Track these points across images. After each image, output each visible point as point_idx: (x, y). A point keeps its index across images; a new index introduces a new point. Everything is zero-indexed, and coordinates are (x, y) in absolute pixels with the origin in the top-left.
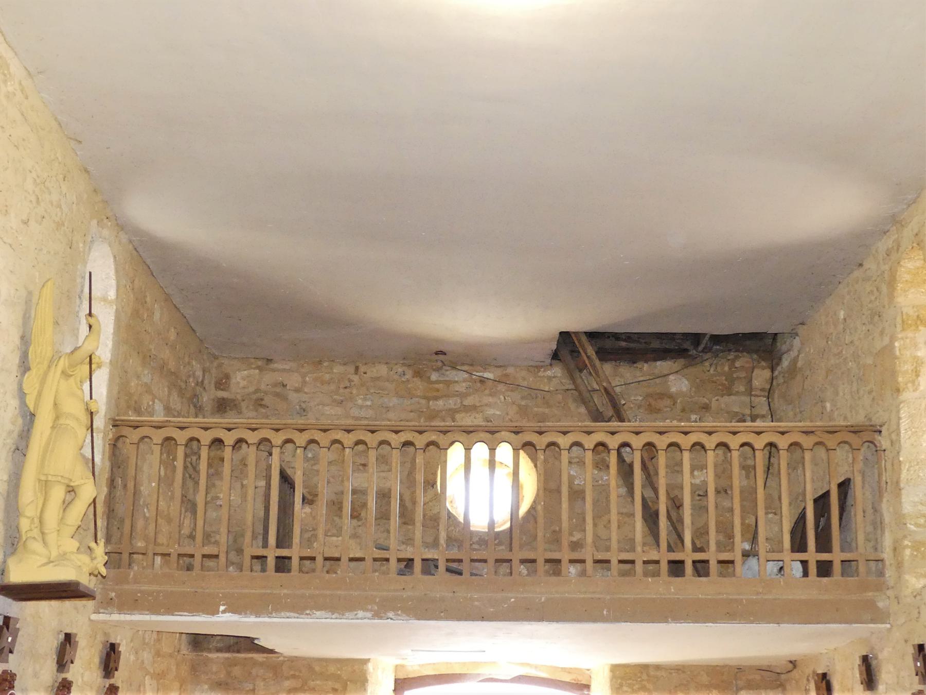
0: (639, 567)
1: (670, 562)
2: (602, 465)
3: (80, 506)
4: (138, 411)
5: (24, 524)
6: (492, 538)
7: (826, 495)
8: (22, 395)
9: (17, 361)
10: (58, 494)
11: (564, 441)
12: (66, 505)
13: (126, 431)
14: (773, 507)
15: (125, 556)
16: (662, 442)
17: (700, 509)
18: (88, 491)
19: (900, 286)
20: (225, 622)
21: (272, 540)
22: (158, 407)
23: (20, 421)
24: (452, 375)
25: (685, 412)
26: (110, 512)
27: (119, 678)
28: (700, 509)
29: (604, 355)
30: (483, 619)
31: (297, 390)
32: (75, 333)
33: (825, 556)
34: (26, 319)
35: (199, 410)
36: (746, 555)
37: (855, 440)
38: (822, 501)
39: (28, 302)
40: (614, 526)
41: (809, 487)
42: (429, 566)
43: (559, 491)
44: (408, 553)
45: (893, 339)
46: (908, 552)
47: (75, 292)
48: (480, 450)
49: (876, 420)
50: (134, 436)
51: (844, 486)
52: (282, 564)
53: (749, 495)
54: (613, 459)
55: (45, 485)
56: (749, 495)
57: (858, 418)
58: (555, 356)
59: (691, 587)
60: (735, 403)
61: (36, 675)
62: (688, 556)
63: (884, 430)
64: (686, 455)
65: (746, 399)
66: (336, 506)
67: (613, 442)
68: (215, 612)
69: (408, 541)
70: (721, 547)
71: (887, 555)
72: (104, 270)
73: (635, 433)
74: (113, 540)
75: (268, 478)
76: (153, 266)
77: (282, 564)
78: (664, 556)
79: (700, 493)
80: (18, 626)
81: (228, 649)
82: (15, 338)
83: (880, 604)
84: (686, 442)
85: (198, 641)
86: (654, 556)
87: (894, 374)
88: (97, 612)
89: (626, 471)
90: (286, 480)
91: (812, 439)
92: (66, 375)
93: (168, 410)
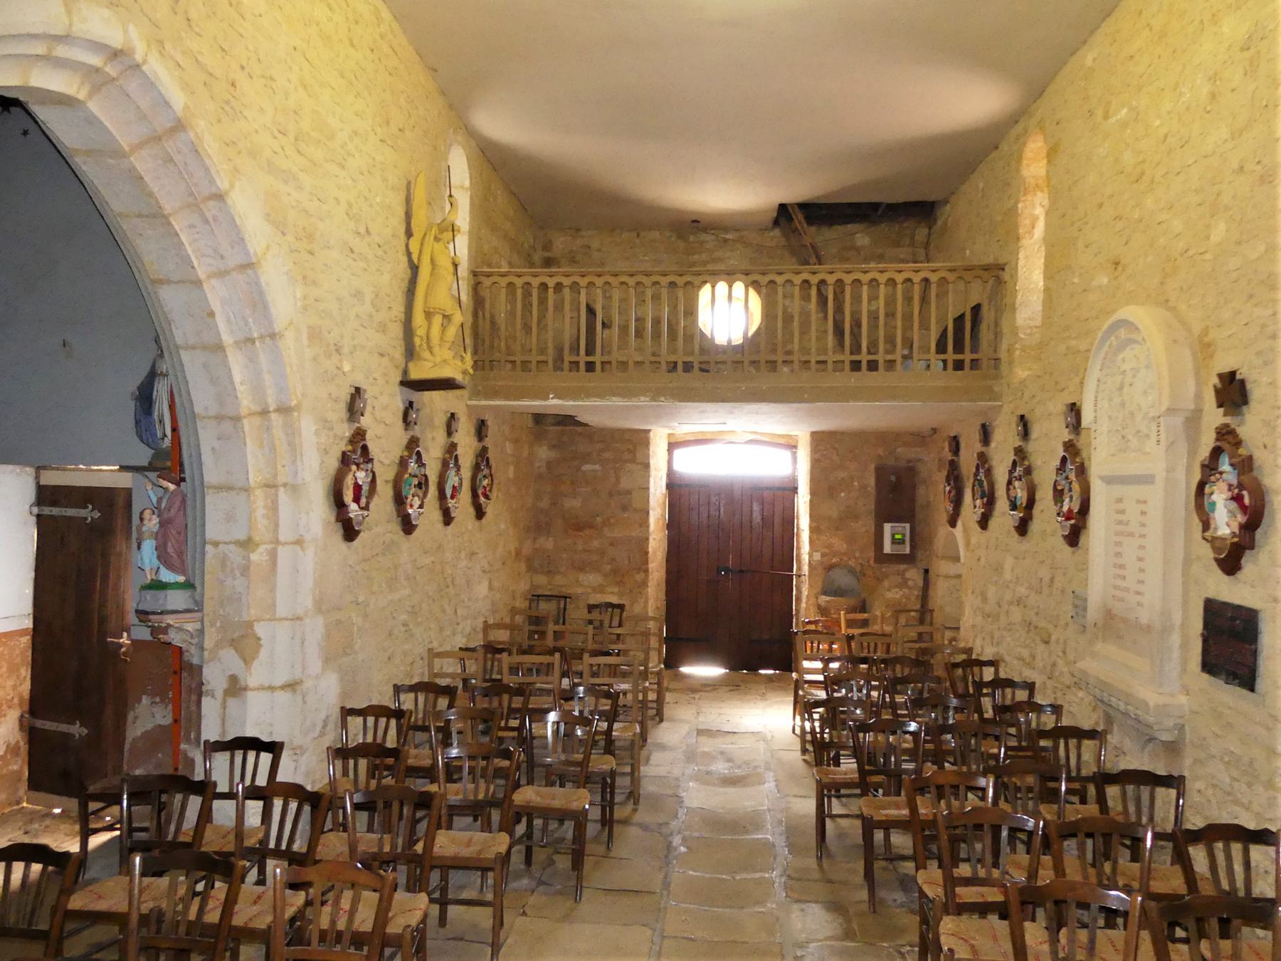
0: (830, 366)
1: (852, 362)
2: (806, 298)
3: (452, 331)
4: (489, 266)
5: (417, 341)
6: (731, 349)
7: (962, 317)
8: (409, 254)
9: (403, 230)
10: (437, 320)
11: (780, 280)
12: (444, 328)
13: (482, 279)
14: (925, 326)
15: (487, 363)
16: (848, 279)
17: (874, 326)
18: (458, 318)
19: (1025, 162)
20: (553, 404)
21: (582, 351)
22: (504, 263)
23: (409, 271)
24: (704, 237)
25: (866, 260)
26: (476, 335)
27: (488, 442)
28: (874, 326)
29: (810, 220)
30: (723, 401)
31: (599, 250)
32: (443, 208)
33: (959, 357)
34: (408, 201)
35: (532, 265)
36: (905, 357)
37: (985, 274)
38: (959, 320)
39: (408, 189)
40: (814, 339)
41: (950, 309)
42: (688, 367)
43: (776, 317)
44: (672, 358)
45: (1017, 202)
46: (1017, 352)
47: (441, 180)
48: (722, 287)
49: (1001, 261)
50: (487, 282)
51: (976, 309)
52: (590, 367)
53: (908, 317)
54: (814, 292)
55: (428, 315)
56: (908, 317)
57: (990, 260)
58: (776, 222)
59: (866, 378)
60: (903, 252)
61: (433, 439)
62: (864, 357)
63: (1007, 268)
64: (865, 288)
65: (910, 250)
66: (624, 329)
67: (814, 280)
68: (547, 398)
69: (673, 350)
70: (887, 352)
71: (1003, 355)
72: (460, 167)
73: (830, 274)
74: (480, 351)
75: (579, 311)
76: (495, 162)
77: (590, 367)
78: (847, 357)
79: (874, 317)
80: (1222, 410)
81: (558, 424)
82: (400, 212)
83: (996, 389)
84: (865, 278)
85: (539, 418)
86: (841, 358)
87: (1016, 227)
88: (470, 399)
89: (823, 300)
90: (591, 311)
91: (955, 275)
92: (437, 239)
93: (511, 264)
